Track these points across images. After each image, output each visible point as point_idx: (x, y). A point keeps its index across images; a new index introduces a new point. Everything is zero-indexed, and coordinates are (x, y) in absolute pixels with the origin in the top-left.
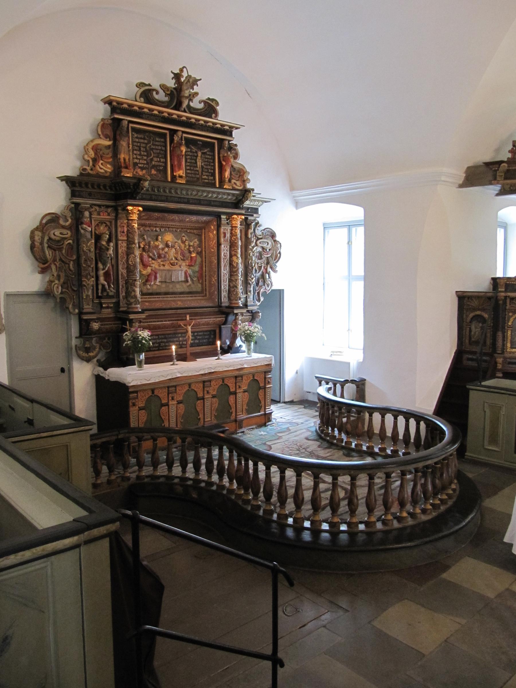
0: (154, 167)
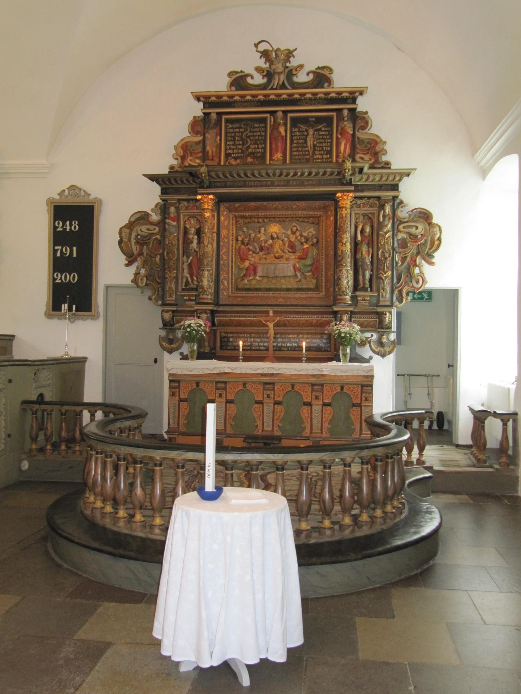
0: (249, 155)
